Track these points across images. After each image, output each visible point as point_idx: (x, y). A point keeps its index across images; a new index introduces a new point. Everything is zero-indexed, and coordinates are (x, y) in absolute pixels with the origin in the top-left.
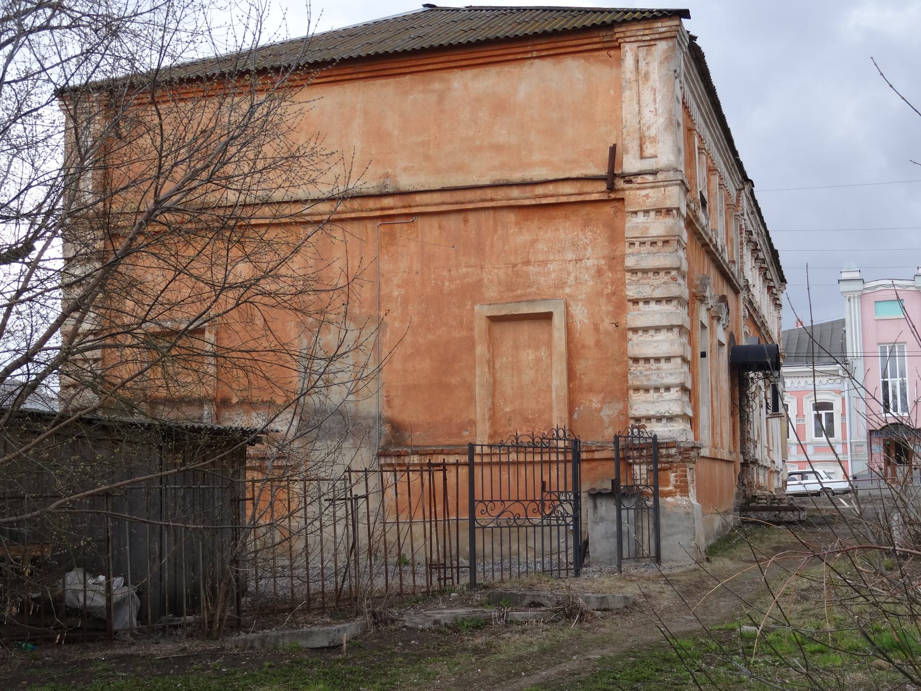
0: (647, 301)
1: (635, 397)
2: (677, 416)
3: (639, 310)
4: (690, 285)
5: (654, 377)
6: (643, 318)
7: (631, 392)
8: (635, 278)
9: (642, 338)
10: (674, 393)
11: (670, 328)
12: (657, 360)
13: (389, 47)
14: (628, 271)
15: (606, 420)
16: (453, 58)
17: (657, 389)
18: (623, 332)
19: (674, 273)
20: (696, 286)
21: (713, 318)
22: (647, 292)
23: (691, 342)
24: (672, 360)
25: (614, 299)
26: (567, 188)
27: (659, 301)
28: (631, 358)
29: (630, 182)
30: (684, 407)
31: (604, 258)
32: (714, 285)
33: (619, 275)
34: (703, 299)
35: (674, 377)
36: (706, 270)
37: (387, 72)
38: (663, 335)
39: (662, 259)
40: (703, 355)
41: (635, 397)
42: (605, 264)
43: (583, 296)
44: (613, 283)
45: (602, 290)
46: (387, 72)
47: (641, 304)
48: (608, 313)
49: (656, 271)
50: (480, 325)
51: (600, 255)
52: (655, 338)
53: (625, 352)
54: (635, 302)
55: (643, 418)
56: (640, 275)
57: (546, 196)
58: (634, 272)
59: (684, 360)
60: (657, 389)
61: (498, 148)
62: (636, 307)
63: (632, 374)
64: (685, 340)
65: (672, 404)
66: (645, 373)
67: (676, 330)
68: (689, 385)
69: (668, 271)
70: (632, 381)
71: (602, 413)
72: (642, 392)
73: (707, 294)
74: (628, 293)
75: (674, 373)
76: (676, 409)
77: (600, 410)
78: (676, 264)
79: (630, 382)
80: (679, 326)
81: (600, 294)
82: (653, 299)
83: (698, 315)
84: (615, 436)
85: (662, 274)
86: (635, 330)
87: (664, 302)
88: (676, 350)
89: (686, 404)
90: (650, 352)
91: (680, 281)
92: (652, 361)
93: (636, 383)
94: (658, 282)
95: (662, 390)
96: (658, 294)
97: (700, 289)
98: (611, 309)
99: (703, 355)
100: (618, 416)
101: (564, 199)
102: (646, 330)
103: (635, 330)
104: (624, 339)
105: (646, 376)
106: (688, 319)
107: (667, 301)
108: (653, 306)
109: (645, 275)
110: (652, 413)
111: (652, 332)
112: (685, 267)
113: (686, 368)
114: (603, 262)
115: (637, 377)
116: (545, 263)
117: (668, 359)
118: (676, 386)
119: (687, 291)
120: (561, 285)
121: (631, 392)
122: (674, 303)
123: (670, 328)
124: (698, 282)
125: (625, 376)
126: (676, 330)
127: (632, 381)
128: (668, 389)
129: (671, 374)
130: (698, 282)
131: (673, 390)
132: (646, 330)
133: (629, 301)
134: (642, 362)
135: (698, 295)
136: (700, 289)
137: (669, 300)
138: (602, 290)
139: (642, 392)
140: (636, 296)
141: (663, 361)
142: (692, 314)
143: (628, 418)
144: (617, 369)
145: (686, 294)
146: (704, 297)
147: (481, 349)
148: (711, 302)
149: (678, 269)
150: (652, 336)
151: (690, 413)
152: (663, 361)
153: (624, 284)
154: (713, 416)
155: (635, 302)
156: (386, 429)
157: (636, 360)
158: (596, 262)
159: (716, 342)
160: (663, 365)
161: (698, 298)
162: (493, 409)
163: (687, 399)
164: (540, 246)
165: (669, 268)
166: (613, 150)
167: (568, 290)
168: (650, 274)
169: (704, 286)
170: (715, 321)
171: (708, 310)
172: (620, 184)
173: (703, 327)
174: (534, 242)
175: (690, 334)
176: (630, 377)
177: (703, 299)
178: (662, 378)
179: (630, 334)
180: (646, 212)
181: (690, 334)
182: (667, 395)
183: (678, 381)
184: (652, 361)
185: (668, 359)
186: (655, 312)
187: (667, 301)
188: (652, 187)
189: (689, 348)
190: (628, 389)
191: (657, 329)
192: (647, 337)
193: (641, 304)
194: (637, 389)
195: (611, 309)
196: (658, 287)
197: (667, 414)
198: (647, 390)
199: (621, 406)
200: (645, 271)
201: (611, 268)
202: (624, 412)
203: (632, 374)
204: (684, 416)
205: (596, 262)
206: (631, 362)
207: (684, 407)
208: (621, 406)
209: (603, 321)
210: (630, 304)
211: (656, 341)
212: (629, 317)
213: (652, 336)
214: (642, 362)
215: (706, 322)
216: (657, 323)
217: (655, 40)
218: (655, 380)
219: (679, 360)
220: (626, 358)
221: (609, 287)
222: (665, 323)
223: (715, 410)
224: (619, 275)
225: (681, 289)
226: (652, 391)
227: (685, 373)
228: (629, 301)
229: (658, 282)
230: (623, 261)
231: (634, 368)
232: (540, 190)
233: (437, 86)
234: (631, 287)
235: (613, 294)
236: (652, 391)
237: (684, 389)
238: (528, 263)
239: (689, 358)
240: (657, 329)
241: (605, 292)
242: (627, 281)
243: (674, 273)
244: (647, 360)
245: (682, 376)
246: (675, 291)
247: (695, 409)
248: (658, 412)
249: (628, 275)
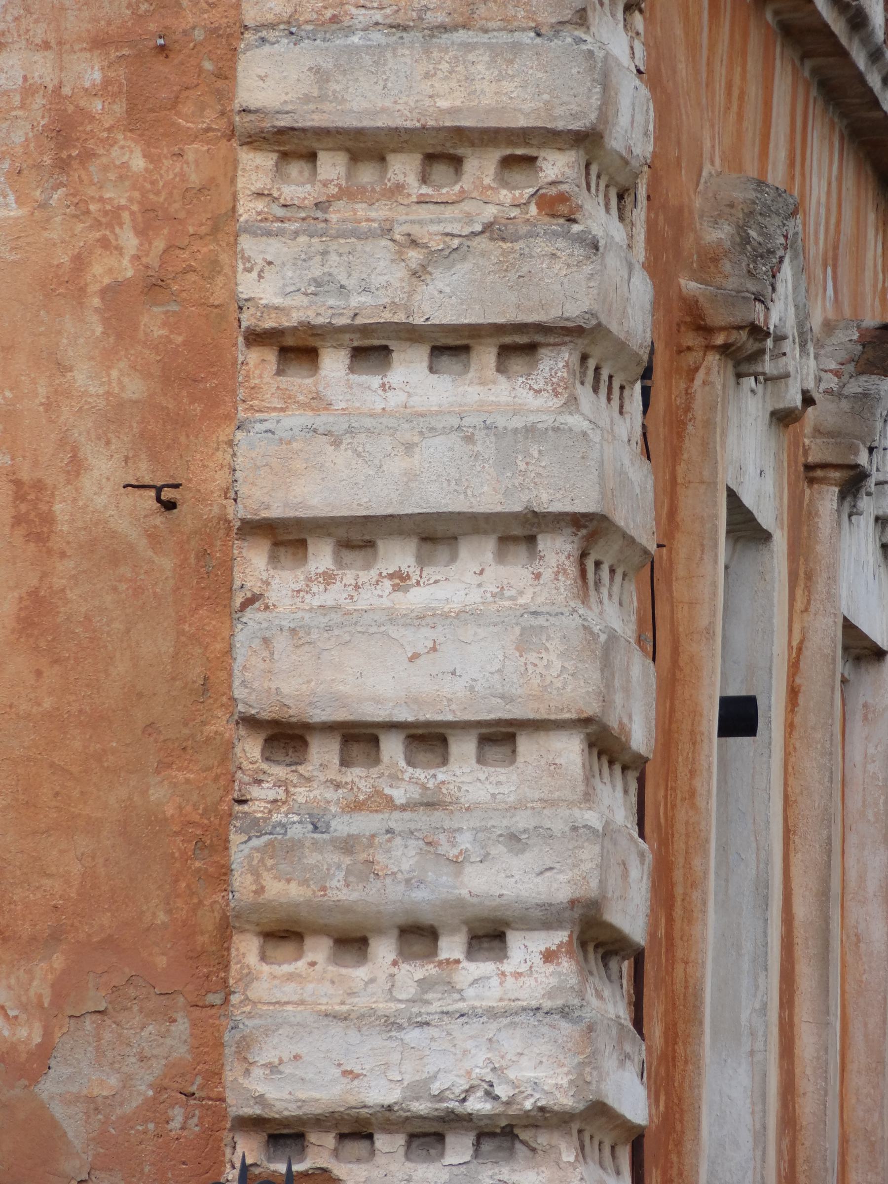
0: (371, 349)
1: (278, 986)
2: (546, 1119)
3: (318, 402)
4: (664, 255)
5: (403, 857)
6: (339, 459)
7: (247, 949)
8: (298, 188)
9: (335, 595)
10: (531, 968)
11: (519, 532)
12: (429, 739)
13: (845, 1109)
14: (257, 140)
15: (74, 1126)
17: (418, 936)
18: (210, 544)
19: (557, 166)
20: (709, 261)
21: (813, 472)
22: (374, 285)
23: (656, 632)
24: (525, 745)
25: (153, 322)
27: (450, 346)
28: (251, 722)
30: (591, 1060)
31: (99, 43)
32: (832, 259)
33: (195, 164)
34: (748, 351)
35: (531, 859)
36: (779, 154)
38: (470, 579)
39: (481, 65)
40: (739, 717)
41: (278, 986)
42: (105, 89)
44: (150, 219)
45: (80, 262)
47: (334, 364)
48: (115, 414)
49: (443, 150)
51: (76, 23)
52: (416, 598)
53: (212, 686)
54: (297, 348)
55: (321, 1122)
56: (332, 167)
58: (295, 145)
59: (605, 746)
60: (418, 936)
62: (298, 382)
63: (255, 827)
64: (615, 613)
65: (511, 1042)
66: (342, 826)
67: (557, 550)
68: (631, 918)
69: (518, 150)
70: (257, 878)
71: (48, 1088)
72: (318, 951)
73: (780, 314)
74: (248, 285)
75: (532, 834)
76: (539, 1073)
77: (40, 1060)
78: (573, 109)
79: (242, 882)
80: (577, 521)
81: (65, 285)
82: (411, 334)
83: (708, 451)
84: (122, 248)
85: (481, 167)
86: (287, 537)
87: (486, 357)
88: (557, 679)
89: (605, 1043)
90: (379, 684)
91: (598, 218)
92: (392, 748)
93: (285, 891)
94: (452, 220)
95: (452, 947)
96: (445, 300)
97: (732, 276)
98: (135, 388)
99: (739, 717)
100: (154, 1109)
102: (358, 536)
103: (287, 537)
104: (214, 593)
105: (347, 845)
106: (639, 476)
107: (506, 352)
108: (411, 378)
109: (367, 175)
110: (378, 1093)
111: (398, 556)
112: (632, 130)
113: (614, 803)
114: (90, 72)
115: (293, 848)
117: (499, 737)
118: (545, 918)
119: (641, 290)
121: (247, 949)
122: (555, 363)
123: (519, 532)
124: (719, 234)
125: (208, 840)
126: (557, 550)
127: (257, 878)
128: (489, 935)
129: (515, 840)
130: (719, 234)
131: (525, 949)
132: (358, 536)
133: (257, 338)
134: (323, 753)
135: (718, 316)
136: (732, 276)
137: (519, 344)
138: (80, 262)
139: (318, 951)
140: (300, 311)
141: (464, 749)
142: (669, 441)
143: (222, 1122)
144: (158, 793)
145: (634, 312)
146: (757, 332)
148: (802, 370)
149: (586, 140)
150: (400, 580)
151: (633, 1102)
152: (464, 749)
153: (224, 224)
154: (789, 1121)
155: (297, 348)
157: (286, 737)
158: (43, 69)
159: (825, 637)
160: (465, 773)
161: (713, 336)
163: (614, 1006)
165: (524, 135)
168: (404, 169)
169: (761, 258)
170: (828, 499)
171: (783, 419)
173: (745, 528)
175: (652, 576)
176: (241, 850)
177: (748, 351)
178: (457, 864)
179: (254, 564)
181: (652, 576)
182: (482, 980)
183: (559, 887)
184: (392, 748)
185: (499, 737)
186: (425, 423)
187: (506, 352)
189: (639, 671)
190: (226, 929)
191: (436, 534)
192: (369, 587)
193: (334, 364)
194: (285, 933)
195: (135, 388)
196: (451, 253)
197: (477, 1105)
198: (352, 942)
199: (177, 1039)
200: (366, 147)
201: (146, 116)
202: (198, 1082)
203: (255, 827)
204: (592, 1121)
205: (43, 69)
206: (250, 749)
207: (591, 1060)
208: (177, 1039)
209: (76, 466)
210: (260, 364)
211: (421, 618)
212: (251, 448)
213: (400, 580)
214: (323, 753)
215: (765, 500)
216: (436, 497)
218: (408, 877)
219: (570, 750)
220: (221, 725)
221: (129, 240)
222: (487, 496)
223: (807, 1085)
224: (195, 164)
225: (607, 277)
226: (384, 950)
227: (607, 833)
228: (257, 338)
229: (452, 220)
230: (226, 74)
231: (270, 788)
234: (273, 248)
235: (154, 286)
236: (384, 950)
237: (596, 939)
239: (640, 738)
240: (436, 534)
241: (102, 271)
242: (248, 209)
243: (557, 166)
244: (360, 739)
245: (590, 854)
246: (554, 284)
247: (671, 1077)
248: (418, 1089)
249: (256, 168)
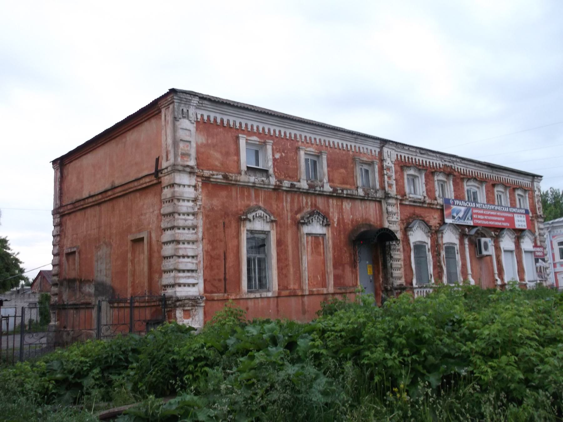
1: (165, 276)
12: (170, 257)
16: (126, 127)
26: (147, 180)
29: (162, 173)
37: (113, 137)
43: (154, 229)
46: (113, 137)
50: (130, 244)
57: (143, 184)
61: (136, 164)
70: (163, 269)
101: (148, 184)
103: (164, 243)
116: (145, 214)
120: (149, 224)
147: (129, 255)
156: (111, 291)
162: (133, 282)
164: (145, 207)
166: (157, 160)
167: (151, 226)
172: (160, 175)
174: (144, 204)
180: (167, 186)
188: (168, 175)
194: (165, 272)
217: (169, 105)
232: (141, 182)
233: (124, 140)
238: (142, 215)
